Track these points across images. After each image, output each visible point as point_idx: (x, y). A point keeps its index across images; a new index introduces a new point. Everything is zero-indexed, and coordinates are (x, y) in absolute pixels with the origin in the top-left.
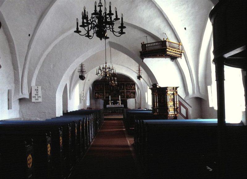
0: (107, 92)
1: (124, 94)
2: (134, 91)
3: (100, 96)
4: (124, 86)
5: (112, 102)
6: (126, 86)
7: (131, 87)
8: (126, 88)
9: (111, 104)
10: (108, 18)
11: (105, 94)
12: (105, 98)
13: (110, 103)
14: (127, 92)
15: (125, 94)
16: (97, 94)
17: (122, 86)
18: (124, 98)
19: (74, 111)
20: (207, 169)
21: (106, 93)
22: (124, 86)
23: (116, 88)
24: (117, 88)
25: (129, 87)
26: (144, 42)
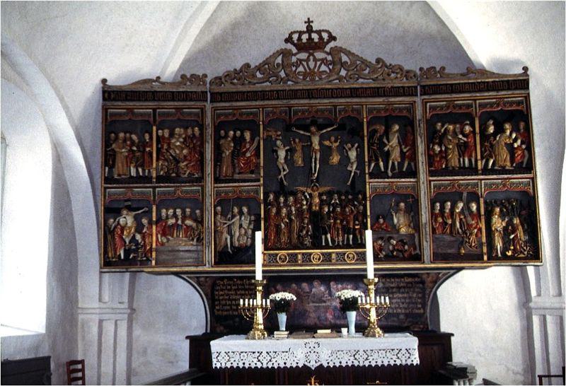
0: (240, 201)
1: (416, 224)
2: (519, 179)
3: (155, 238)
4: (408, 139)
5: (281, 306)
6: (434, 137)
7: (489, 151)
8: (431, 158)
9: (271, 327)
10: (304, 205)
11: (209, 218)
12: (209, 255)
13: (259, 317)
14: (439, 197)
15: (425, 216)
16: (127, 219)
17: (387, 133)
18: (418, 258)
19: (236, 334)
20: (419, 363)
21: (225, 205)
22: (408, 139)
23: (326, 152)
24: (335, 159)
25: (464, 149)
26: (422, 66)
